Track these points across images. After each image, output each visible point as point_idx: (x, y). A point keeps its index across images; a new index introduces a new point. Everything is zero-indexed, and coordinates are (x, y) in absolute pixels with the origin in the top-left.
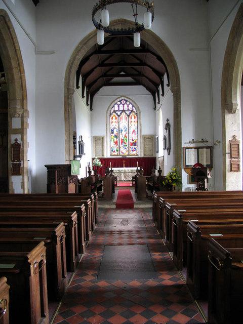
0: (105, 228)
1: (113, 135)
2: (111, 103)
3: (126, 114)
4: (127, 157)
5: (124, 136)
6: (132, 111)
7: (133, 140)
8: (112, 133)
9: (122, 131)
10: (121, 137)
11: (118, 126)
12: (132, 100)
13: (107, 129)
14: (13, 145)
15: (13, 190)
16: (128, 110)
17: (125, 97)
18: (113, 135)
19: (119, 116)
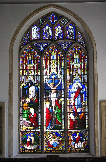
0: (48, 114)
1: (28, 100)
2: (23, 23)
3: (60, 48)
4: (62, 156)
5: (53, 104)
6: (75, 40)
7: (76, 114)
8: (26, 94)
9: (49, 91)
10: (47, 104)
11: (38, 78)
12: (75, 16)
13: (11, 85)
14: (46, 141)
15: (4, 155)
16: (65, 37)
17: (59, 7)
18: (28, 100)
19: (41, 53)
